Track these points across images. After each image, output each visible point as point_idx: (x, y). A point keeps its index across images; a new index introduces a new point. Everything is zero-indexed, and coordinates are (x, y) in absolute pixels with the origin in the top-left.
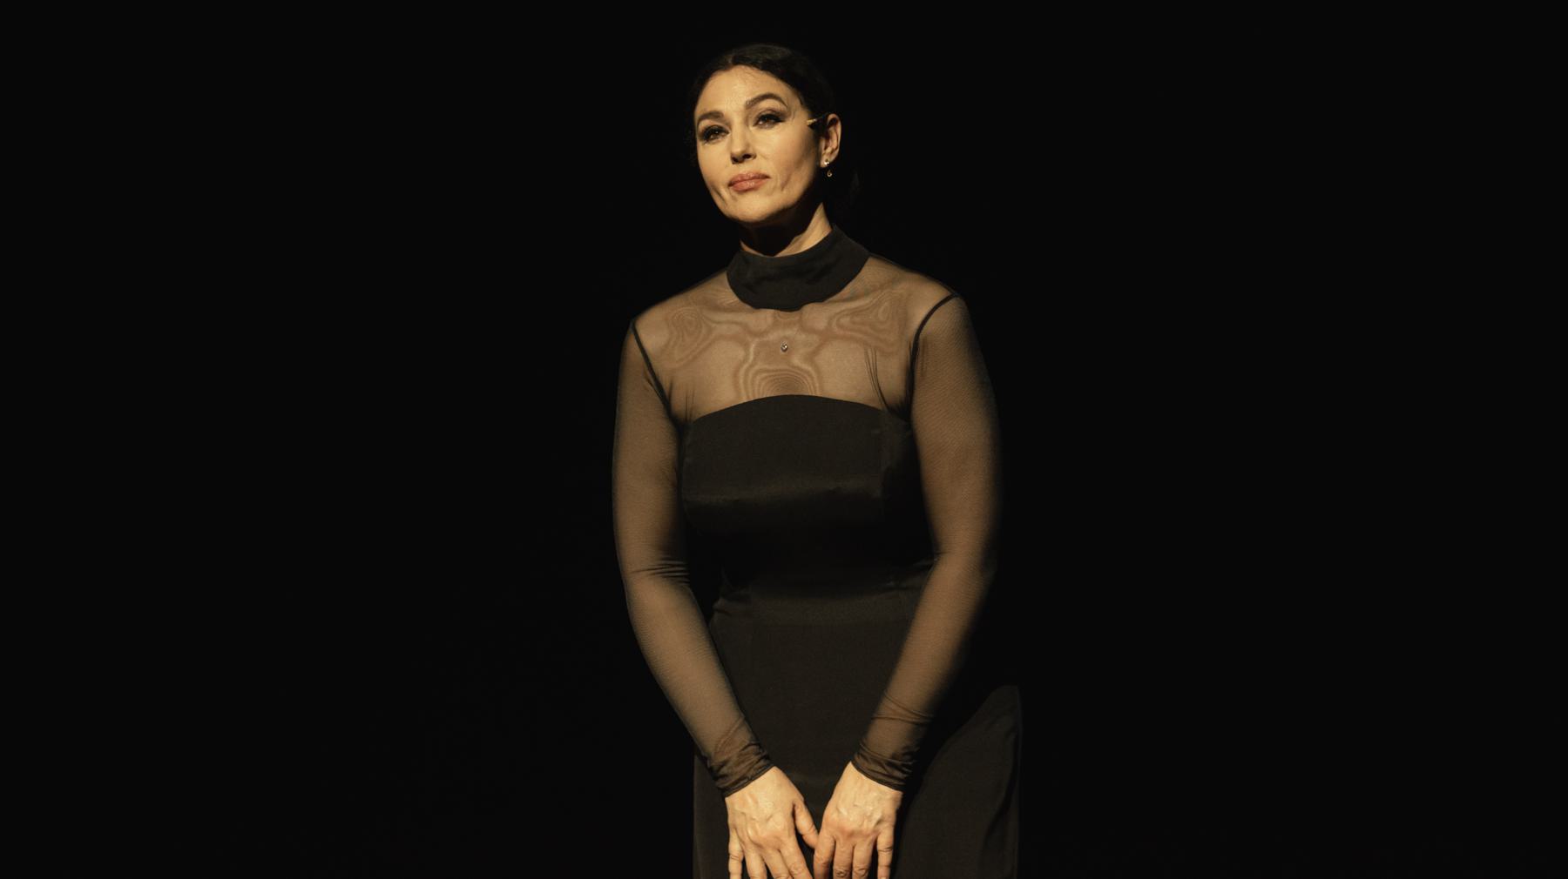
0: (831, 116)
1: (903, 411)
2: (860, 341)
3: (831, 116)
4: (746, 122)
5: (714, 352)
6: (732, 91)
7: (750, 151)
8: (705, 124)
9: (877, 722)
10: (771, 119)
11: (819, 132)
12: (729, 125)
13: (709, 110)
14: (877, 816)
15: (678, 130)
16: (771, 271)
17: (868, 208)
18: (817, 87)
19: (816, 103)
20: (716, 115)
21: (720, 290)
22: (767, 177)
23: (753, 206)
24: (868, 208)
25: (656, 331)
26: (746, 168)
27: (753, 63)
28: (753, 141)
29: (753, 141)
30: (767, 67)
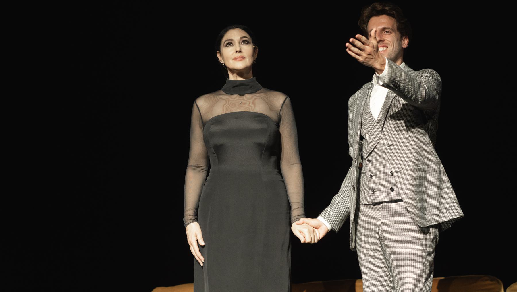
1: (278, 124)
4: (239, 43)
5: (209, 106)
6: (235, 35)
8: (227, 42)
9: (395, 26)
10: (248, 43)
12: (235, 42)
16: (239, 89)
17: (263, 75)
18: (256, 37)
19: (254, 43)
20: (232, 40)
21: (221, 92)
23: (240, 65)
24: (263, 75)
25: (203, 104)
26: (238, 55)
28: (236, 52)
29: (236, 52)
30: (244, 29)
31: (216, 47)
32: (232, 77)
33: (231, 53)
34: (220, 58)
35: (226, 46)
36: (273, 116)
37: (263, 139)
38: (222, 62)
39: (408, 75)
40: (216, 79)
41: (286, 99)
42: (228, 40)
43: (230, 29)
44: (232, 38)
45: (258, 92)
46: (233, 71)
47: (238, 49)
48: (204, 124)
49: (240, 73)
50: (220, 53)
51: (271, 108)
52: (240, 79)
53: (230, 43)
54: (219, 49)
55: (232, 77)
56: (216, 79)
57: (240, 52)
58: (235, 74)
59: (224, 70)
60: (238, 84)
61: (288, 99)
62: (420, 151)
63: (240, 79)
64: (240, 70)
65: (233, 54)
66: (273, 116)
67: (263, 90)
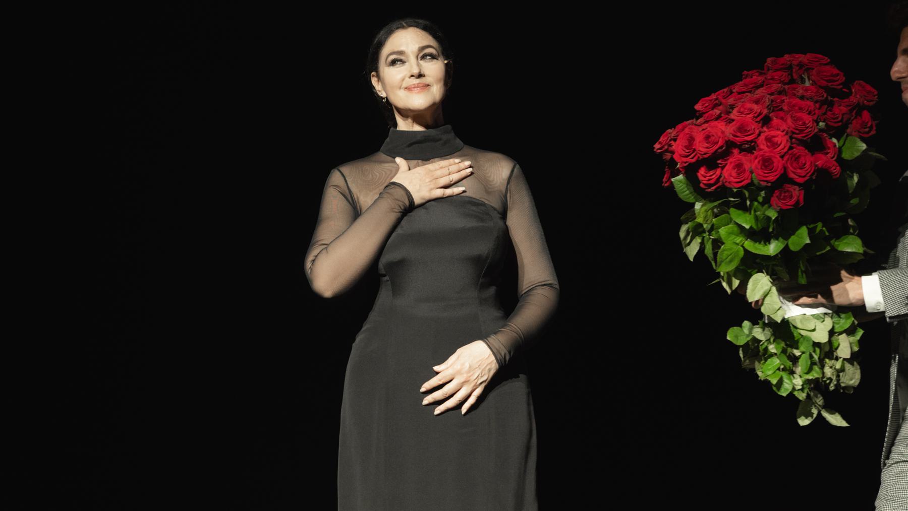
6: (407, 40)
10: (433, 57)
12: (407, 57)
13: (396, 50)
14: (484, 378)
15: (367, 60)
16: (420, 150)
17: (457, 123)
18: (451, 45)
20: (401, 53)
21: (381, 156)
23: (419, 101)
24: (457, 123)
26: (415, 81)
27: (417, 27)
28: (409, 71)
29: (409, 71)
30: (425, 29)
31: (370, 62)
32: (403, 125)
33: (399, 77)
34: (378, 87)
35: (393, 63)
37: (484, 247)
38: (383, 95)
39: (437, 373)
40: (369, 129)
41: (512, 171)
43: (398, 28)
44: (402, 48)
45: (804, 300)
46: (406, 113)
47: (416, 71)
48: (431, 190)
49: (416, 116)
50: (378, 76)
51: (487, 187)
52: (418, 128)
54: (376, 69)
55: (403, 125)
56: (369, 129)
57: (420, 76)
58: (410, 120)
59: (385, 111)
60: (419, 138)
63: (418, 128)
64: (421, 111)
65: (403, 80)
66: (494, 202)
67: (467, 149)
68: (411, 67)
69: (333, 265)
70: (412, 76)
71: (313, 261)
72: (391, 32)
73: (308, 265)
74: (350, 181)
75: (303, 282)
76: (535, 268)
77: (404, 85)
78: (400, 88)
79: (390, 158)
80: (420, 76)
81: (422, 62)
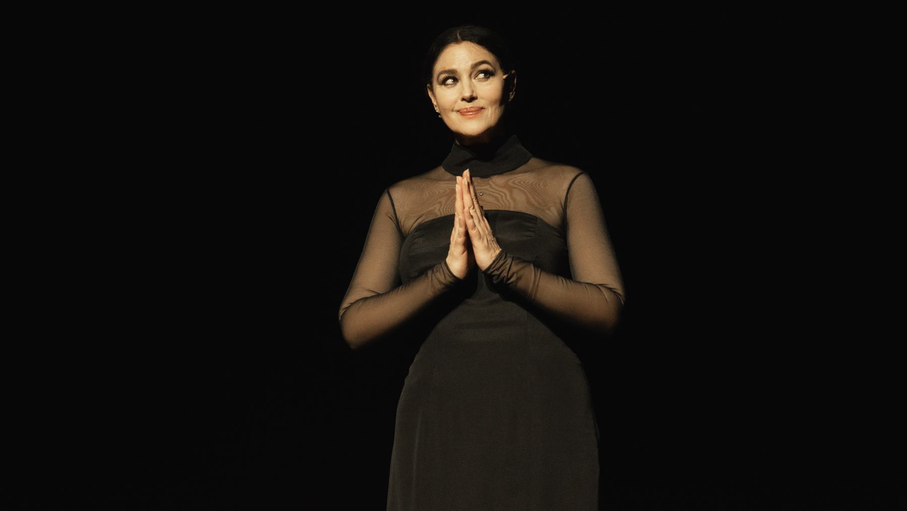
0: (513, 72)
1: (563, 227)
2: (552, 188)
3: (513, 72)
4: (470, 75)
6: (460, 56)
7: (474, 95)
8: (443, 76)
10: (488, 74)
11: (506, 87)
13: (448, 68)
15: (421, 73)
16: (484, 155)
18: (506, 54)
19: (505, 70)
21: (441, 171)
22: (482, 108)
26: (475, 104)
27: (471, 40)
28: (466, 87)
29: (466, 87)
30: (481, 42)
35: (444, 82)
36: (551, 215)
40: (434, 148)
42: (445, 72)
44: (454, 67)
47: (467, 94)
50: (432, 90)
53: (453, 77)
54: (431, 83)
56: (434, 148)
61: (583, 184)
62: (526, 172)
66: (551, 215)
67: (534, 162)
68: (463, 88)
69: (372, 302)
70: (463, 99)
71: (347, 308)
72: (442, 45)
73: (341, 312)
74: (405, 202)
75: (335, 325)
76: (594, 260)
77: (456, 108)
78: (452, 111)
79: (449, 175)
80: (472, 99)
81: (473, 81)
